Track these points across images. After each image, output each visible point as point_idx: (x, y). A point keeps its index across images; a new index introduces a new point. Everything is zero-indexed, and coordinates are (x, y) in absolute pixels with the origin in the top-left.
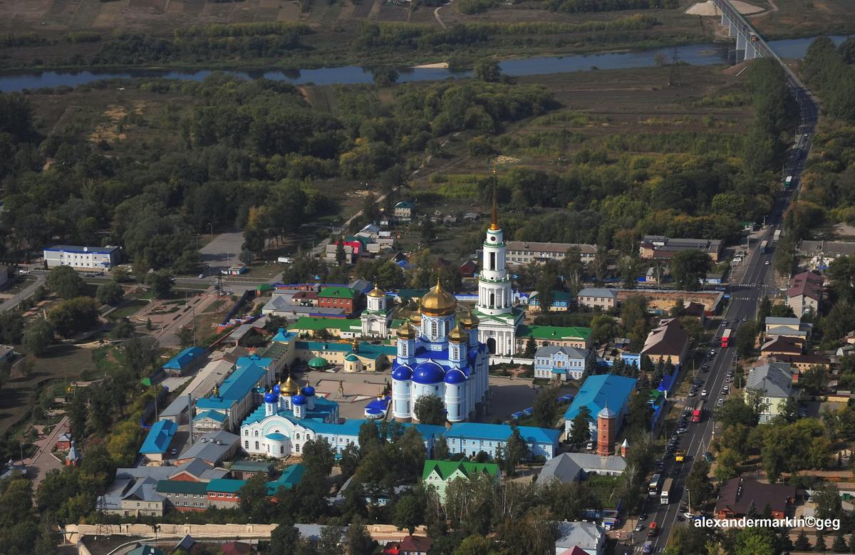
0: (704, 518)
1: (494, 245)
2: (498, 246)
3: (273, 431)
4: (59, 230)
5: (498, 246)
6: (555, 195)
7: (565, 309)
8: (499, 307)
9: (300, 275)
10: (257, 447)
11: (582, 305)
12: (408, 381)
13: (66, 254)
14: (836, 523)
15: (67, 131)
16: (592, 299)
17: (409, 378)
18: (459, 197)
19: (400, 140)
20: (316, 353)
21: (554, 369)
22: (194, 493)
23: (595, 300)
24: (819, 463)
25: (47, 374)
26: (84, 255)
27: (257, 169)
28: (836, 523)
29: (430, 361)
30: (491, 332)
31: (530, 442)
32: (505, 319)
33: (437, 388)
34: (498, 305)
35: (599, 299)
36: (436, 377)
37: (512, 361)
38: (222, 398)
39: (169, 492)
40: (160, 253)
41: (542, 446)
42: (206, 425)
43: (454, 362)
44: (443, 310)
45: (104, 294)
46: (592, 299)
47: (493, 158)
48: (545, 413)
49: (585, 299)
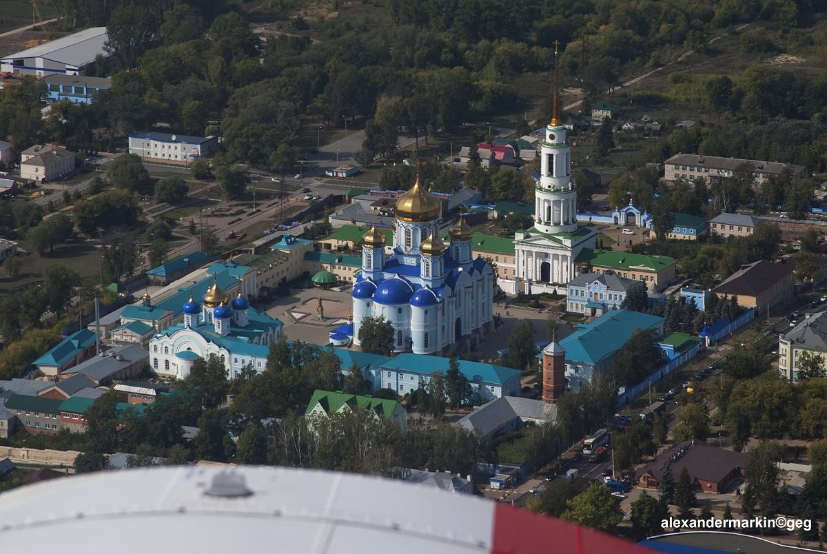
0: (671, 518)
1: (552, 145)
2: (557, 146)
3: (183, 349)
4: (157, 115)
5: (557, 146)
6: (802, 103)
7: (693, 237)
8: (557, 224)
9: (401, 180)
10: (167, 367)
11: (715, 234)
12: (369, 300)
13: (152, 142)
14: (807, 523)
15: (273, 6)
16: (727, 227)
17: (370, 296)
18: (688, 100)
19: (658, 30)
20: (327, 267)
21: (589, 301)
22: (47, 413)
23: (731, 228)
24: (812, 432)
25: (35, 276)
26: (172, 145)
27: (450, 56)
28: (807, 523)
29: (397, 277)
30: (547, 255)
31: (475, 381)
32: (560, 238)
33: (400, 311)
34: (556, 221)
35: (736, 228)
36: (401, 297)
37: (555, 291)
38: (154, 307)
39: (19, 408)
40: (254, 146)
41: (489, 387)
42: (124, 338)
43: (424, 280)
44: (419, 214)
45: (163, 189)
46: (727, 227)
47: (771, 56)
48: (522, 350)
49: (719, 226)
